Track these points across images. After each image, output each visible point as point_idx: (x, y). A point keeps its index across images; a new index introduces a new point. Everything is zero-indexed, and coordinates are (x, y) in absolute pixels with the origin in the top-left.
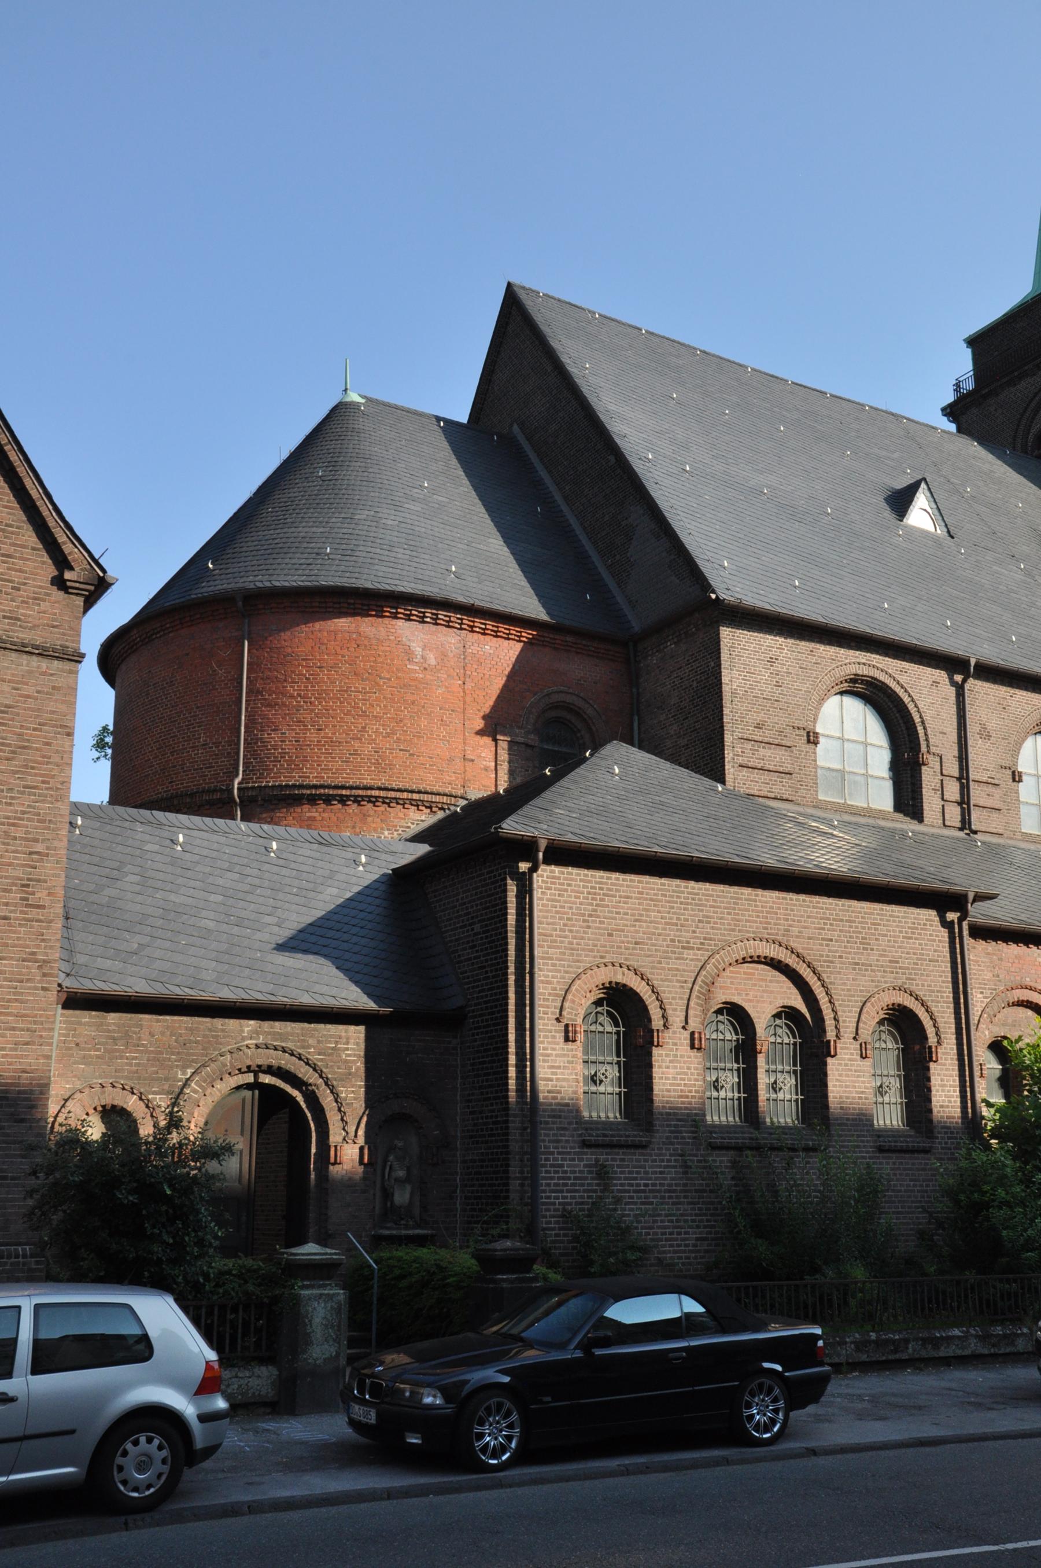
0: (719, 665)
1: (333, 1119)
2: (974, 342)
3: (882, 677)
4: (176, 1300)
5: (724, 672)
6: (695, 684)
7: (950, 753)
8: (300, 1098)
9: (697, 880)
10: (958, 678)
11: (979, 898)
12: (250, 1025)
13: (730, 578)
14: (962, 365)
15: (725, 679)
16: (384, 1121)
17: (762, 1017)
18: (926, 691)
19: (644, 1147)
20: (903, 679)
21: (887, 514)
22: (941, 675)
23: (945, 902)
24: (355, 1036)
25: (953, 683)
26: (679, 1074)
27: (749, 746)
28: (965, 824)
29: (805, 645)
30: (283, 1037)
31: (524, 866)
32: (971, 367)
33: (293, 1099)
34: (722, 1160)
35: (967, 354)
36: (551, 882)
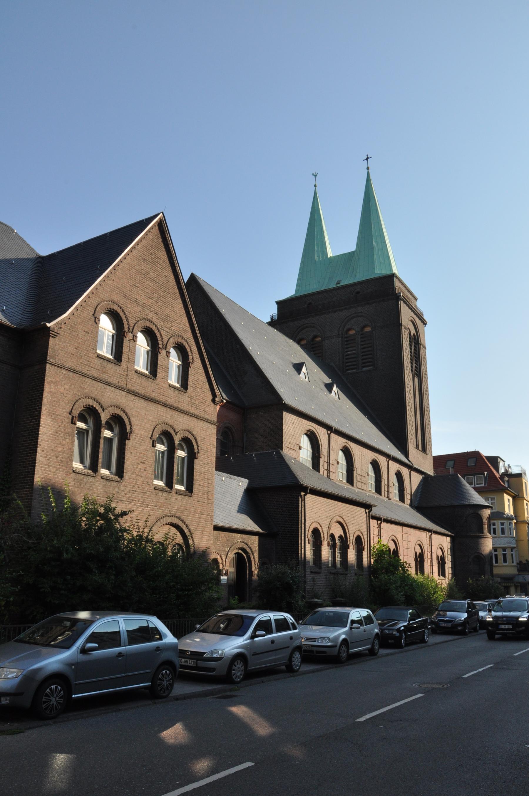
0: (282, 423)
1: (253, 563)
2: (279, 303)
3: (314, 430)
4: (158, 618)
5: (284, 426)
6: (271, 427)
7: (326, 455)
8: (245, 555)
9: (329, 499)
10: (329, 432)
11: (375, 506)
12: (239, 535)
13: (288, 399)
14: (274, 310)
15: (284, 428)
16: (262, 564)
17: (337, 536)
18: (322, 433)
19: (319, 573)
20: (318, 431)
21: (294, 372)
22: (325, 430)
23: (367, 506)
24: (256, 538)
25: (328, 434)
26: (326, 553)
27: (288, 449)
28: (328, 476)
29: (300, 419)
30: (244, 539)
31: (303, 494)
32: (276, 312)
33: (244, 557)
34: (332, 576)
35: (276, 306)
36: (310, 499)
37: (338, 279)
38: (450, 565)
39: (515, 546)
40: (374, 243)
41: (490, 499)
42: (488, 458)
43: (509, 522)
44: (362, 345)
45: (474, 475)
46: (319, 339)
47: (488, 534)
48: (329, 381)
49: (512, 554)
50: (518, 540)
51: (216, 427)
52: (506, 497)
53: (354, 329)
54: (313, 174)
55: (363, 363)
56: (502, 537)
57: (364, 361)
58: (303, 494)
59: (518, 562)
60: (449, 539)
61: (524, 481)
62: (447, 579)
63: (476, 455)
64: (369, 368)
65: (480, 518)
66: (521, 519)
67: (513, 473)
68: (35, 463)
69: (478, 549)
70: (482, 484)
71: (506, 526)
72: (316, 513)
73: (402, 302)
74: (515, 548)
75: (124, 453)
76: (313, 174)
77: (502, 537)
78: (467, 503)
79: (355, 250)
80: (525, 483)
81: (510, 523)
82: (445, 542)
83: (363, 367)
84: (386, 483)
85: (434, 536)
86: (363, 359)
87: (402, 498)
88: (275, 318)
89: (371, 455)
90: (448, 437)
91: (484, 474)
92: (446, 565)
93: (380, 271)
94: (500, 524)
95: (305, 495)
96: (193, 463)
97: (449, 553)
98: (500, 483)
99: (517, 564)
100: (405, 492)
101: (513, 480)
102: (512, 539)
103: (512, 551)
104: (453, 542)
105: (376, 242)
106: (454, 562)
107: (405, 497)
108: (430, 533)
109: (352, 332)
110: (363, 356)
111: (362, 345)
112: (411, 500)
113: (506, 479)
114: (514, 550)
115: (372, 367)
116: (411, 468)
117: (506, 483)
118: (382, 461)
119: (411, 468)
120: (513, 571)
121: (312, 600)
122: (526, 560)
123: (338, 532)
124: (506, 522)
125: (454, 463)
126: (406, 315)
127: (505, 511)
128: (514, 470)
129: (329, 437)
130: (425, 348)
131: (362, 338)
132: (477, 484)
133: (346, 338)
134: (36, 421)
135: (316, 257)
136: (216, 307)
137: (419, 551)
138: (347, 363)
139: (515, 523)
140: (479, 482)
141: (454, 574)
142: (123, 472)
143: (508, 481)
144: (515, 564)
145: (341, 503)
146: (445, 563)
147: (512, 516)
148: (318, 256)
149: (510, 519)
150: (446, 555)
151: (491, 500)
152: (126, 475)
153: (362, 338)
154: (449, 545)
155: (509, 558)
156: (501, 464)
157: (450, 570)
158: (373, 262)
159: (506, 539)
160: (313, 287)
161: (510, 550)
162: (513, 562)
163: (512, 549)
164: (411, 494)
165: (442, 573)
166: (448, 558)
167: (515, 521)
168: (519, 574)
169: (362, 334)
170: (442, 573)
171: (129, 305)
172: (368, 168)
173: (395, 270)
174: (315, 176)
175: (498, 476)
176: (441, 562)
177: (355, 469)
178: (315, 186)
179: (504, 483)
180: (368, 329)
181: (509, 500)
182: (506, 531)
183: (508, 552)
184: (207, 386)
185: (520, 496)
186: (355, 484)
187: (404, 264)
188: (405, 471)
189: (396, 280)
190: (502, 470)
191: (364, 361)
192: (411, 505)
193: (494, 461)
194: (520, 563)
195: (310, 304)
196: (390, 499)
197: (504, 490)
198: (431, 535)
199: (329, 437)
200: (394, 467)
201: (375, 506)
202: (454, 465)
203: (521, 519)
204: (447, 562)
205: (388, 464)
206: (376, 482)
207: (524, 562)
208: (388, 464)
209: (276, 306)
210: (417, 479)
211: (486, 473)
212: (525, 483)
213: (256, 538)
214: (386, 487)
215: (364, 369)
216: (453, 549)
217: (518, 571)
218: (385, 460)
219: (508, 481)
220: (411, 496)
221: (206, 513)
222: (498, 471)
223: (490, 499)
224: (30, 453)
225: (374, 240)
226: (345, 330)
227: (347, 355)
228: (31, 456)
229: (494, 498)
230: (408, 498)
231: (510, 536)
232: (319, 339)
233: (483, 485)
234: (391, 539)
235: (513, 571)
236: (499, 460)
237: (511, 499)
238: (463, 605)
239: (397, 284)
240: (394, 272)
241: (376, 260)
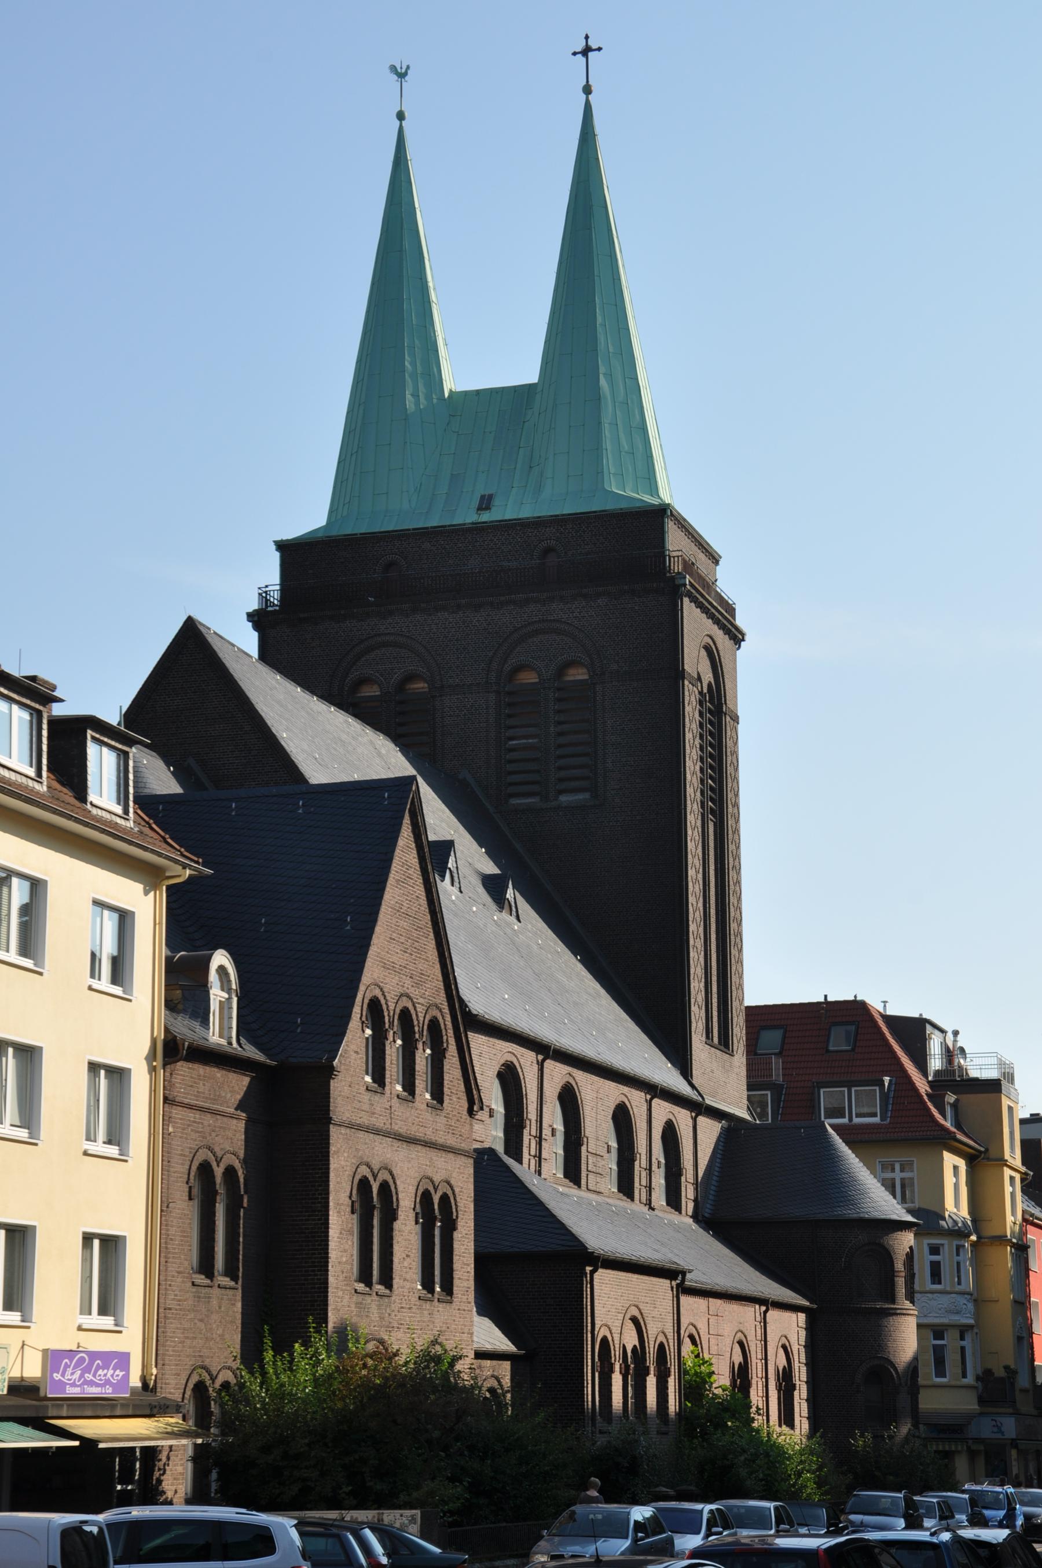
10: (540, 1057)
14: (268, 573)
24: (507, 1365)
31: (588, 1269)
32: (277, 581)
35: (274, 560)
37: (481, 490)
38: (804, 1395)
39: (972, 1322)
40: (603, 382)
41: (897, 1167)
42: (893, 1022)
43: (955, 1243)
44: (560, 723)
45: (849, 1085)
46: (420, 686)
47: (908, 1304)
48: (491, 868)
49: (963, 1349)
50: (979, 1300)
51: (471, 1161)
52: (950, 1160)
53: (534, 669)
54: (393, 69)
55: (561, 780)
56: (932, 1292)
57: (563, 774)
58: (588, 1269)
59: (980, 1372)
60: (802, 1317)
61: (1005, 1102)
62: (797, 1431)
63: (853, 1014)
64: (580, 796)
65: (886, 1257)
66: (990, 1230)
67: (974, 1074)
68: (327, 1288)
69: (879, 1346)
70: (874, 1115)
71: (945, 1258)
72: (613, 1305)
73: (686, 600)
74: (971, 1327)
75: (391, 1246)
76: (393, 69)
77: (932, 1292)
78: (851, 1213)
79: (536, 381)
80: (1010, 1108)
81: (959, 1248)
82: (790, 1328)
83: (561, 792)
84: (644, 1164)
85: (773, 1315)
86: (560, 768)
87: (674, 1200)
88: (275, 597)
89: (614, 1093)
90: (774, 971)
91: (881, 1084)
92: (796, 1393)
93: (622, 490)
94: (926, 1250)
95: (592, 1272)
96: (452, 1239)
97: (803, 1359)
98: (932, 1116)
99: (978, 1378)
100: (683, 1179)
101: (971, 1100)
102: (962, 1300)
103: (962, 1338)
104: (811, 1328)
105: (610, 376)
106: (811, 1383)
107: (683, 1194)
108: (763, 1308)
109: (529, 678)
110: (560, 757)
111: (560, 723)
112: (695, 1201)
113: (951, 1098)
114: (968, 1336)
115: (586, 795)
116: (698, 1108)
117: (948, 1110)
118: (636, 1100)
119: (698, 1108)
120: (966, 1403)
121: (657, 1489)
122: (1007, 1368)
123: (631, 1340)
124: (947, 1245)
125: (784, 1037)
126: (695, 626)
127: (944, 1209)
128: (979, 1068)
129: (541, 1070)
130: (736, 719)
131: (559, 700)
132: (858, 1115)
133: (510, 693)
134: (320, 1220)
135: (408, 397)
136: (266, 724)
137: (738, 1358)
138: (510, 773)
139: (974, 1245)
140: (865, 1110)
141: (814, 1418)
142: (391, 1278)
143: (955, 1106)
144: (970, 1380)
145: (636, 1276)
146: (794, 1387)
147: (964, 1223)
148: (415, 395)
149: (959, 1233)
150: (796, 1365)
151: (902, 1171)
152: (396, 1282)
153: (559, 700)
154: (803, 1334)
155: (952, 1359)
156: (935, 1046)
157: (805, 1405)
158: (598, 449)
159: (945, 1301)
160: (402, 507)
161: (957, 1334)
162: (964, 1376)
163: (963, 1331)
164: (696, 1183)
165: (787, 1418)
166: (800, 1374)
167: (974, 1238)
168: (981, 1414)
169: (559, 689)
170: (787, 1418)
171: (388, 980)
172: (587, 90)
173: (672, 489)
174: (402, 76)
175: (922, 1086)
176: (786, 1379)
177: (585, 1140)
178: (401, 116)
179: (943, 1114)
180: (578, 674)
181: (956, 1168)
182: (946, 1272)
183: (950, 1341)
184: (462, 1087)
185: (992, 1153)
186: (583, 1182)
187: (700, 463)
188: (683, 1118)
189: (670, 526)
190: (936, 1063)
191: (563, 774)
192: (695, 1217)
193: (913, 1032)
194: (985, 1376)
195: (390, 565)
196: (653, 1209)
197: (945, 1141)
198: (765, 1312)
199: (541, 1070)
200: (663, 1110)
201: (690, 1271)
202: (783, 1043)
203: (990, 1230)
204: (798, 1383)
205: (650, 1110)
206: (619, 1164)
207: (1000, 1373)
208: (650, 1110)
209: (277, 555)
210: (710, 1131)
211: (887, 1079)
212: (1010, 1108)
213: (507, 1365)
214: (644, 1174)
215: (564, 799)
216: (811, 1346)
217: (981, 1401)
218: (643, 1101)
219: (955, 1106)
220: (696, 1189)
221: (466, 1331)
222: (922, 1064)
223: (897, 1167)
224: (314, 1271)
225: (602, 369)
226: (507, 667)
227: (511, 750)
228: (316, 1275)
229: (911, 1163)
230: (688, 1193)
231: (958, 1288)
232: (420, 686)
233: (876, 1120)
234: (628, 1316)
235: (966, 1403)
236: (929, 1029)
237: (962, 1164)
238: (762, 1513)
239: (675, 541)
240: (667, 500)
241: (608, 444)
